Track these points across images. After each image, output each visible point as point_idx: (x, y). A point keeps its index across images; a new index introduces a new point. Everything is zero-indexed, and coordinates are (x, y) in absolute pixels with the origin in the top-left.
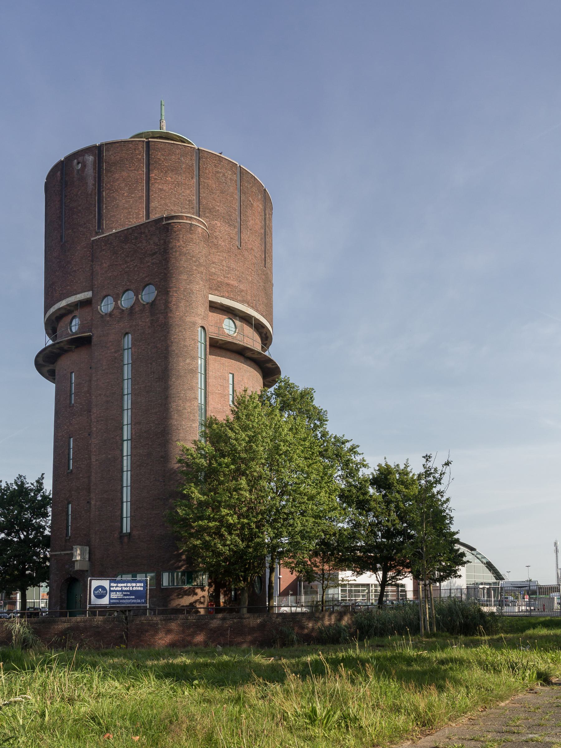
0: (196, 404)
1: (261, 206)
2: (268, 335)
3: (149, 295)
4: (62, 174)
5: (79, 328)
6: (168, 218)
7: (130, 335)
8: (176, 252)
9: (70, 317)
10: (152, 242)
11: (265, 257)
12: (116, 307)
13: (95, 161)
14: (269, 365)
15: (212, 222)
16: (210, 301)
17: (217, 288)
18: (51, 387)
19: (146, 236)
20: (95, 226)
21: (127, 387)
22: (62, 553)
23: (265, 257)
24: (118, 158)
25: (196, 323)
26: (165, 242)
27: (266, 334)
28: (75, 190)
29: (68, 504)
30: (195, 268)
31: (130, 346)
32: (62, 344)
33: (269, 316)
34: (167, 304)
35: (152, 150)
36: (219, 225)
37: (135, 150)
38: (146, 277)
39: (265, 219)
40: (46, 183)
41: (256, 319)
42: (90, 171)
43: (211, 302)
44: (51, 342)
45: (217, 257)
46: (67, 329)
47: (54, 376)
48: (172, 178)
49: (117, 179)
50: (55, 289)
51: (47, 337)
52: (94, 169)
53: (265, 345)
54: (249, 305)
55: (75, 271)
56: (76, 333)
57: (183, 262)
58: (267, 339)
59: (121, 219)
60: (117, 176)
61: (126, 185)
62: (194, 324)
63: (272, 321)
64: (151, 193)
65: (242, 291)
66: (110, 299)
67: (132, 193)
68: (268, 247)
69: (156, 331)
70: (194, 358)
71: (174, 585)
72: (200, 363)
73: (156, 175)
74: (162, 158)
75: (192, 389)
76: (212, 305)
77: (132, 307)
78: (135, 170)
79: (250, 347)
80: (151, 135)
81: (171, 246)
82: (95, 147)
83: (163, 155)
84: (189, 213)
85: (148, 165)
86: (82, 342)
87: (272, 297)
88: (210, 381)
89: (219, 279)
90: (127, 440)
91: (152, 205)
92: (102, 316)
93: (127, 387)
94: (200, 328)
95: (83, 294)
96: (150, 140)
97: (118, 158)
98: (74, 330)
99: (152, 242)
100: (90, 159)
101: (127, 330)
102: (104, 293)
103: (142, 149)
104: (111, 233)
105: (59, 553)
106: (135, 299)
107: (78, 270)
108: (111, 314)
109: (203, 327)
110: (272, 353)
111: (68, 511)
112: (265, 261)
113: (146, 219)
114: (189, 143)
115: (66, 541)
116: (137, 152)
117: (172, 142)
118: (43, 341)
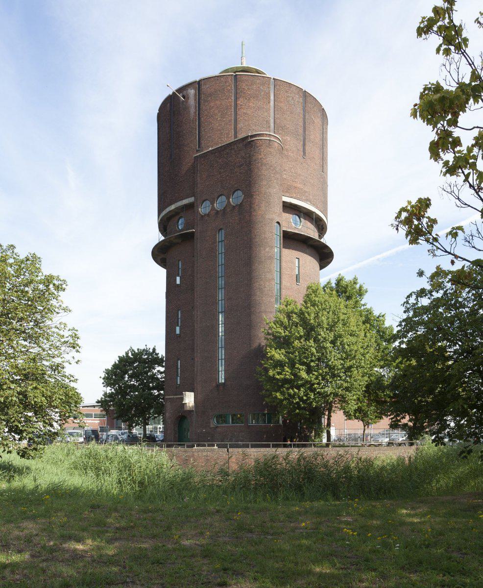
1: (320, 122)
3: (236, 198)
4: (171, 105)
6: (252, 136)
7: (223, 231)
9: (177, 217)
10: (239, 156)
12: (213, 209)
14: (326, 251)
16: (283, 202)
17: (288, 191)
18: (162, 272)
20: (196, 146)
21: (220, 270)
22: (175, 397)
24: (213, 90)
25: (274, 221)
26: (250, 156)
28: (175, 118)
29: (178, 359)
31: (223, 239)
34: (251, 205)
35: (239, 81)
36: (289, 139)
37: (226, 82)
38: (235, 184)
40: (158, 113)
41: (316, 215)
42: (192, 102)
43: (284, 202)
44: (163, 238)
46: (175, 227)
50: (166, 196)
51: (160, 234)
52: (195, 100)
53: (321, 234)
55: (181, 182)
56: (182, 230)
57: (264, 172)
58: (321, 227)
59: (215, 139)
60: (212, 104)
61: (219, 112)
62: (272, 220)
63: (327, 214)
64: (238, 117)
66: (207, 203)
67: (224, 118)
68: (325, 156)
69: (242, 225)
70: (272, 247)
71: (253, 423)
72: (276, 251)
73: (241, 102)
75: (270, 271)
77: (224, 208)
78: (225, 99)
79: (303, 233)
80: (235, 70)
81: (254, 158)
82: (195, 82)
83: (247, 85)
84: (266, 131)
85: (236, 94)
86: (188, 238)
88: (283, 264)
91: (240, 125)
92: (202, 216)
93: (220, 270)
94: (276, 224)
95: (188, 199)
96: (237, 73)
97: (213, 90)
99: (239, 156)
100: (192, 92)
101: (221, 227)
102: (204, 198)
103: (231, 81)
104: (208, 150)
106: (227, 202)
107: (183, 181)
108: (208, 215)
109: (278, 223)
110: (327, 240)
111: (178, 365)
113: (234, 138)
114: (265, 74)
116: (228, 84)
117: (253, 74)
118: (157, 237)
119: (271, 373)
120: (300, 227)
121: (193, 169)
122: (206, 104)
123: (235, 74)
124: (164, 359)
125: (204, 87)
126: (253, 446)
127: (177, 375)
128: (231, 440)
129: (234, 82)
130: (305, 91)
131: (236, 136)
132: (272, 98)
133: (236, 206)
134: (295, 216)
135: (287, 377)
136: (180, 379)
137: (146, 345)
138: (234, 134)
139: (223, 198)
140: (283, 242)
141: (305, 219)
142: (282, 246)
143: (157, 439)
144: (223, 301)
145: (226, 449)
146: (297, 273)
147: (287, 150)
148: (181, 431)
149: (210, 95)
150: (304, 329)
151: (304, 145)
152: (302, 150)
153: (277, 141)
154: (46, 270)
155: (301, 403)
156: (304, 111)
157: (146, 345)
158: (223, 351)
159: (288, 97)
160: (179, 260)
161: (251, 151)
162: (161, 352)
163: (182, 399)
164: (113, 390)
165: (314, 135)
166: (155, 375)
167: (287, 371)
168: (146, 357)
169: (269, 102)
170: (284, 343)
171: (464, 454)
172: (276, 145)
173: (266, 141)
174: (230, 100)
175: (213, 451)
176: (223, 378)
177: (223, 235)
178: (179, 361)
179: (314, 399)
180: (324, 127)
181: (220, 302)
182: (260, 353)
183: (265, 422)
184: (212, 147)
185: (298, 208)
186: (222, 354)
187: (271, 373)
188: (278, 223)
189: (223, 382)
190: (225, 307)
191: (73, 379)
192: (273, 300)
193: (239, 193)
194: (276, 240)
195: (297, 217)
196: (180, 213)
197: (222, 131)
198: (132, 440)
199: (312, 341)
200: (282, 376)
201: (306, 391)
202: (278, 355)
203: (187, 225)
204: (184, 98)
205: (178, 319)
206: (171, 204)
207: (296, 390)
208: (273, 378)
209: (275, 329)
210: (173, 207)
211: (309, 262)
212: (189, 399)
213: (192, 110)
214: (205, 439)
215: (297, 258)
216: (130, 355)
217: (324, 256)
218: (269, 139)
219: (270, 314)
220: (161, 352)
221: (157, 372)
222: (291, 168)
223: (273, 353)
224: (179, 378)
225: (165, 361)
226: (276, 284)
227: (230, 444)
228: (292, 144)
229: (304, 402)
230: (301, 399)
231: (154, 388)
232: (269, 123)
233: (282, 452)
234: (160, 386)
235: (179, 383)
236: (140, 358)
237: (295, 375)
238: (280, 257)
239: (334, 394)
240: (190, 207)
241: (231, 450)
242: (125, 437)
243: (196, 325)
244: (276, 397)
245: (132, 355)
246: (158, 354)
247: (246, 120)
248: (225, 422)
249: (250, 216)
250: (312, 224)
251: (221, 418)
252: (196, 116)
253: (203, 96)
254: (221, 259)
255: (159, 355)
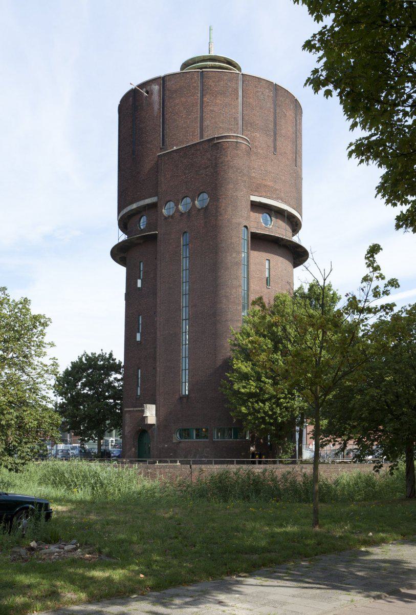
0: (240, 290)
2: (298, 222)
5: (146, 226)
6: (218, 138)
7: (188, 234)
8: (225, 165)
11: (296, 157)
13: (160, 90)
15: (252, 135)
17: (257, 190)
18: (123, 270)
19: (201, 153)
20: (160, 143)
21: (185, 275)
23: (296, 157)
25: (243, 222)
26: (216, 158)
27: (296, 222)
28: (140, 114)
29: (139, 369)
30: (240, 178)
32: (133, 240)
33: (299, 208)
39: (296, 124)
40: (119, 105)
42: (156, 98)
43: (252, 201)
45: (257, 163)
47: (126, 261)
48: (221, 100)
49: (178, 104)
52: (160, 96)
54: (283, 201)
58: (295, 224)
60: (177, 101)
62: (239, 224)
63: (301, 212)
65: (277, 190)
66: (172, 204)
68: (298, 149)
69: (208, 229)
70: (239, 253)
74: (213, 84)
76: (253, 203)
77: (189, 211)
82: (159, 78)
83: (213, 82)
85: (202, 90)
87: (301, 191)
88: (252, 267)
89: (258, 182)
90: (186, 320)
91: (206, 123)
92: (166, 218)
93: (185, 275)
94: (243, 228)
98: (142, 227)
99: (205, 157)
100: (156, 88)
104: (173, 150)
105: (132, 409)
108: (172, 217)
109: (246, 227)
111: (138, 375)
112: (296, 160)
115: (136, 399)
119: (236, 387)
120: (271, 226)
121: (156, 169)
122: (171, 101)
123: (201, 71)
124: (123, 364)
125: (168, 84)
126: (216, 463)
127: (138, 385)
128: (195, 456)
129: (200, 79)
130: (276, 84)
131: (202, 137)
132: (240, 93)
133: (202, 209)
134: (265, 214)
135: (252, 390)
136: (141, 390)
137: (102, 350)
138: (200, 132)
139: (188, 200)
140: (251, 246)
141: (277, 218)
142: (250, 247)
143: (112, 455)
144: (187, 308)
145: (189, 466)
146: (267, 275)
147: (256, 147)
148: (142, 446)
149: (176, 91)
150: (271, 341)
151: (275, 140)
152: (272, 146)
153: (245, 143)
154: (34, 310)
155: (267, 418)
156: (275, 105)
157: (102, 350)
158: (187, 360)
159: (257, 92)
160: (141, 262)
161: (217, 153)
162: (119, 356)
163: (143, 412)
164: (64, 400)
165: (286, 128)
166: (112, 383)
167: (252, 385)
168: (102, 363)
169: (237, 99)
170: (247, 355)
171: (377, 469)
172: (244, 146)
173: (233, 143)
174: (196, 97)
175: (175, 467)
176: (187, 388)
177: (188, 238)
178: (140, 370)
179: (281, 414)
180: (298, 118)
181: (184, 308)
182: (227, 365)
183: (231, 437)
184: (177, 145)
185: (268, 206)
186: (185, 364)
187: (236, 387)
188: (246, 227)
189: (187, 393)
190: (189, 314)
191: (50, 400)
192: (241, 307)
193: (205, 196)
194: (241, 240)
195: (267, 215)
196: (142, 211)
197: (187, 129)
198: (86, 455)
199: (279, 353)
200: (248, 390)
201: (272, 405)
202: (244, 367)
203: (150, 226)
204: (148, 93)
205: (139, 324)
206: (132, 203)
207: (260, 404)
208: (238, 392)
209: (241, 340)
210: (134, 206)
211: (280, 263)
212: (151, 414)
213: (156, 106)
214: (168, 455)
215: (267, 260)
216: (84, 359)
217: (298, 255)
218: (236, 141)
219: (238, 321)
220: (119, 356)
221: (113, 380)
222: (261, 166)
223: (240, 365)
224: (139, 388)
225: (123, 367)
226: (243, 291)
227: (236, 461)
228: (262, 140)
229: (270, 417)
230: (265, 413)
231: (109, 397)
232: (237, 121)
233: (233, 468)
234: (117, 394)
235: (139, 394)
236: (96, 364)
237: (261, 389)
238: (248, 262)
239: (300, 407)
240: (154, 206)
241: (194, 466)
242: (76, 452)
243: (158, 333)
244: (240, 411)
245: (86, 360)
246: (115, 359)
247: (212, 118)
248: (189, 436)
249: (216, 220)
250: (284, 221)
251: (185, 433)
252: (160, 113)
253: (167, 93)
254: (185, 263)
255: (116, 361)
